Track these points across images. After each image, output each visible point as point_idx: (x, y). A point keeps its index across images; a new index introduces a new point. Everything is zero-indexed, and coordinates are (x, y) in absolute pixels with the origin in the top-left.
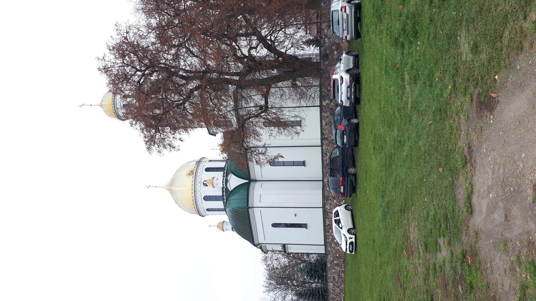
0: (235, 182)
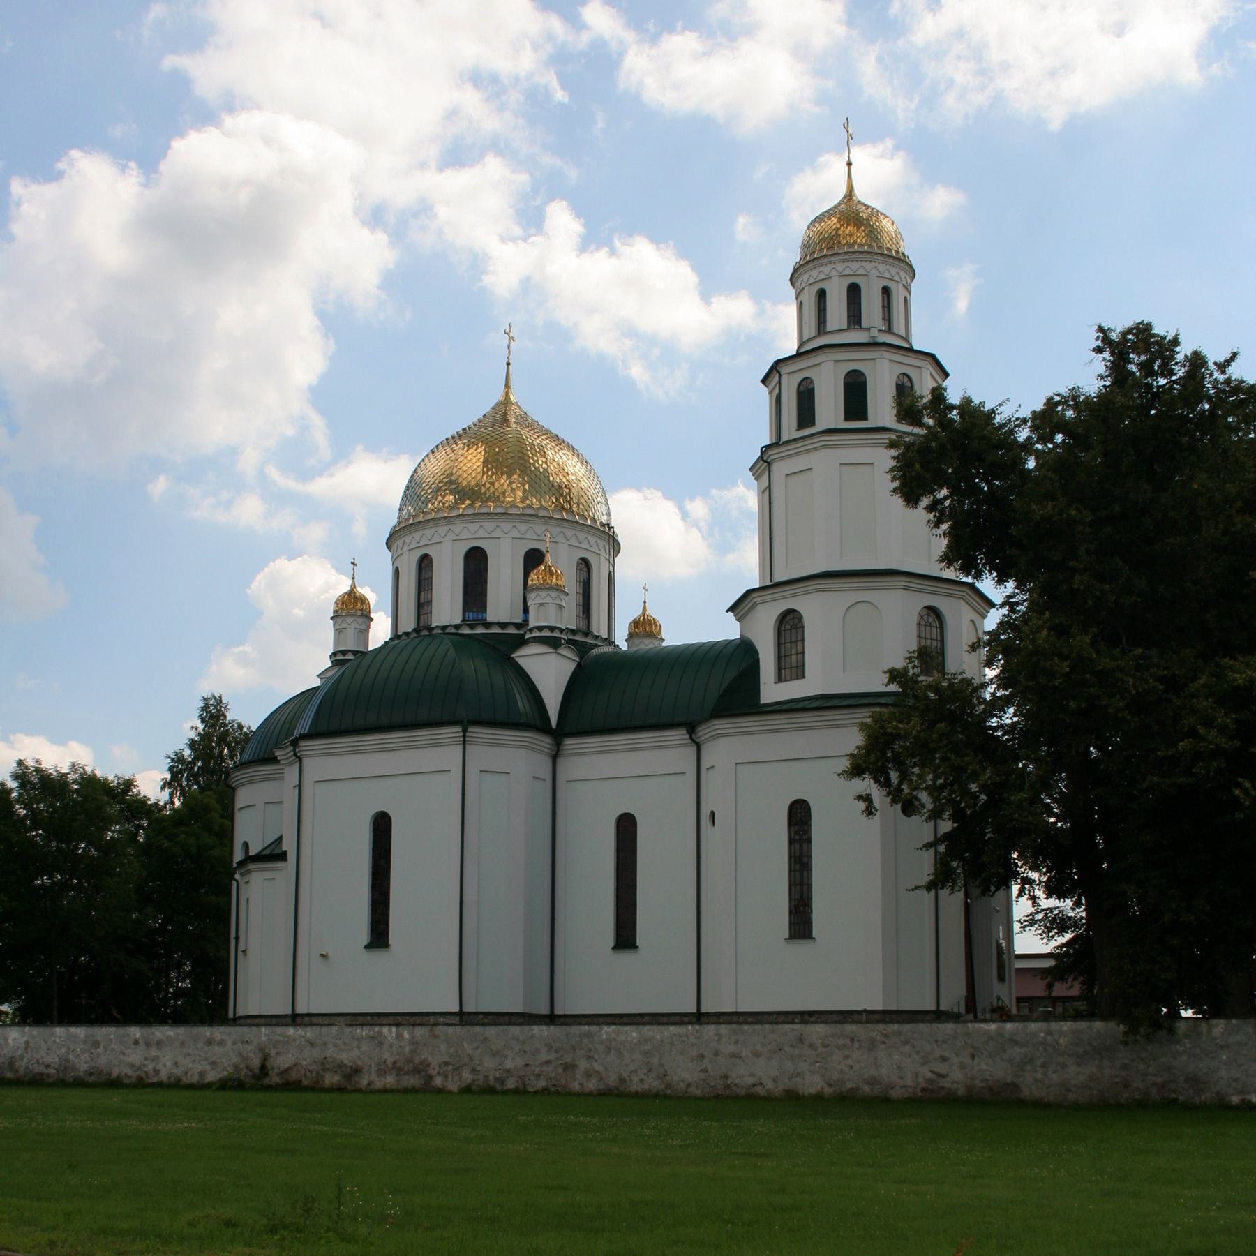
0: (550, 673)
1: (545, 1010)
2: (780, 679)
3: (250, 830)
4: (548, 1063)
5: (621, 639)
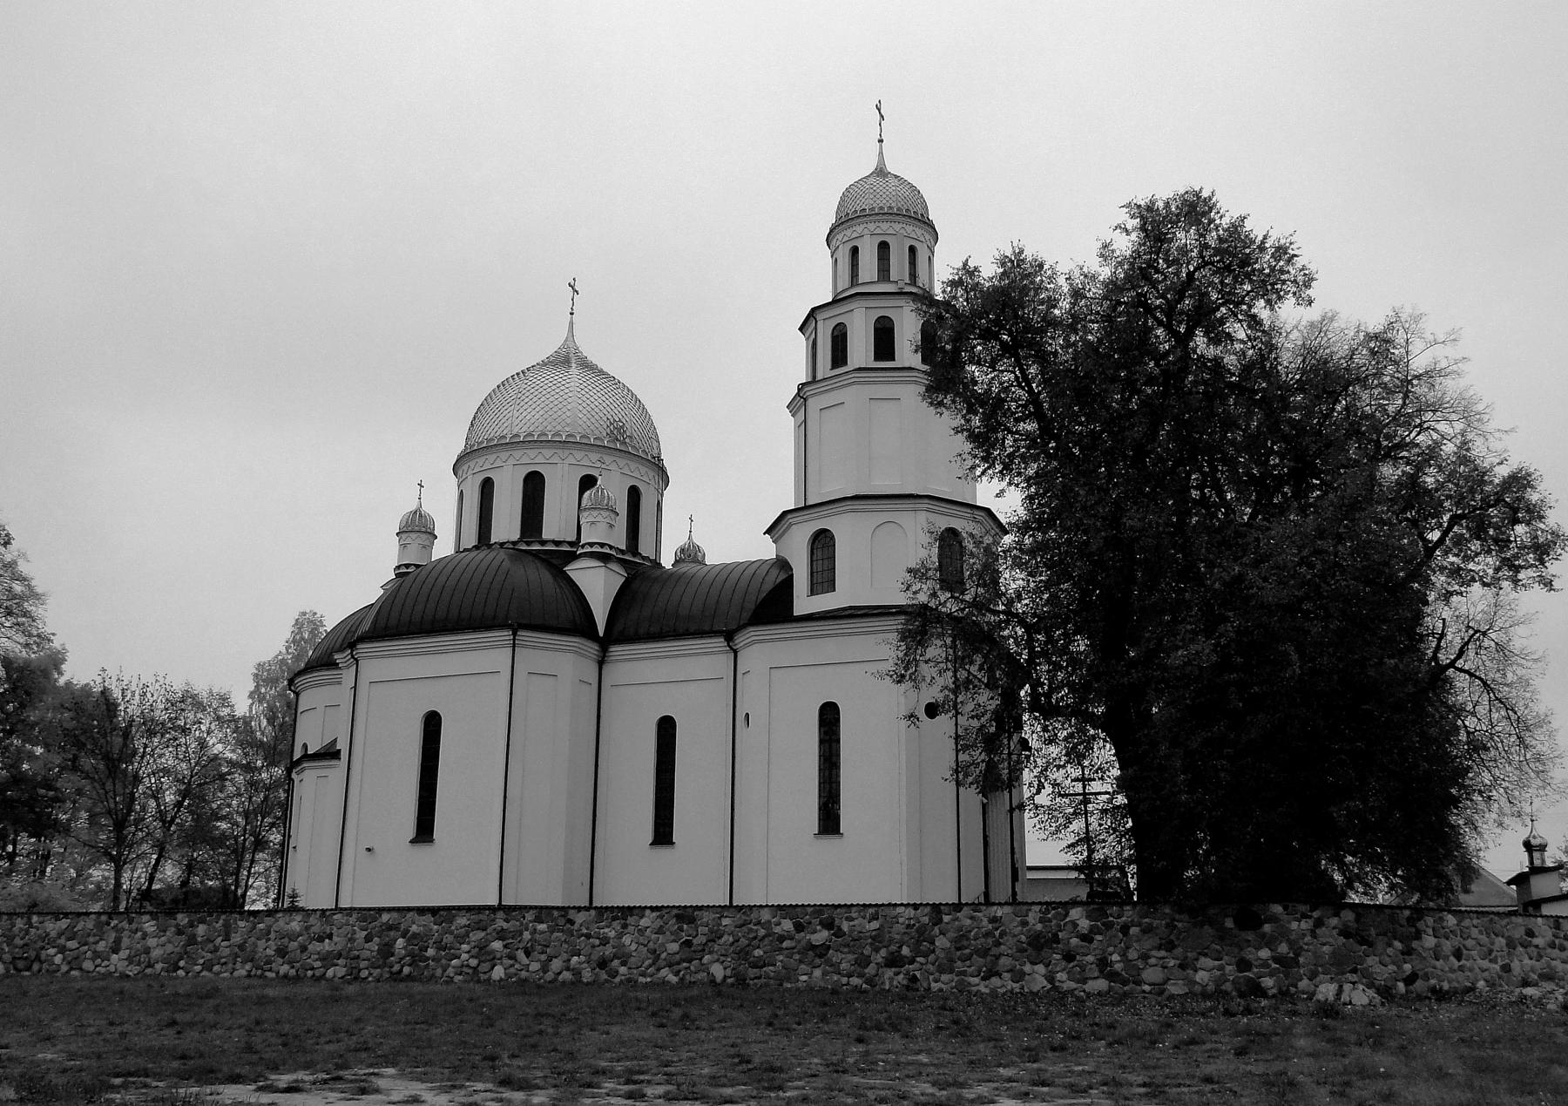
0: (598, 586)
2: (813, 592)
3: (310, 735)
5: (667, 561)
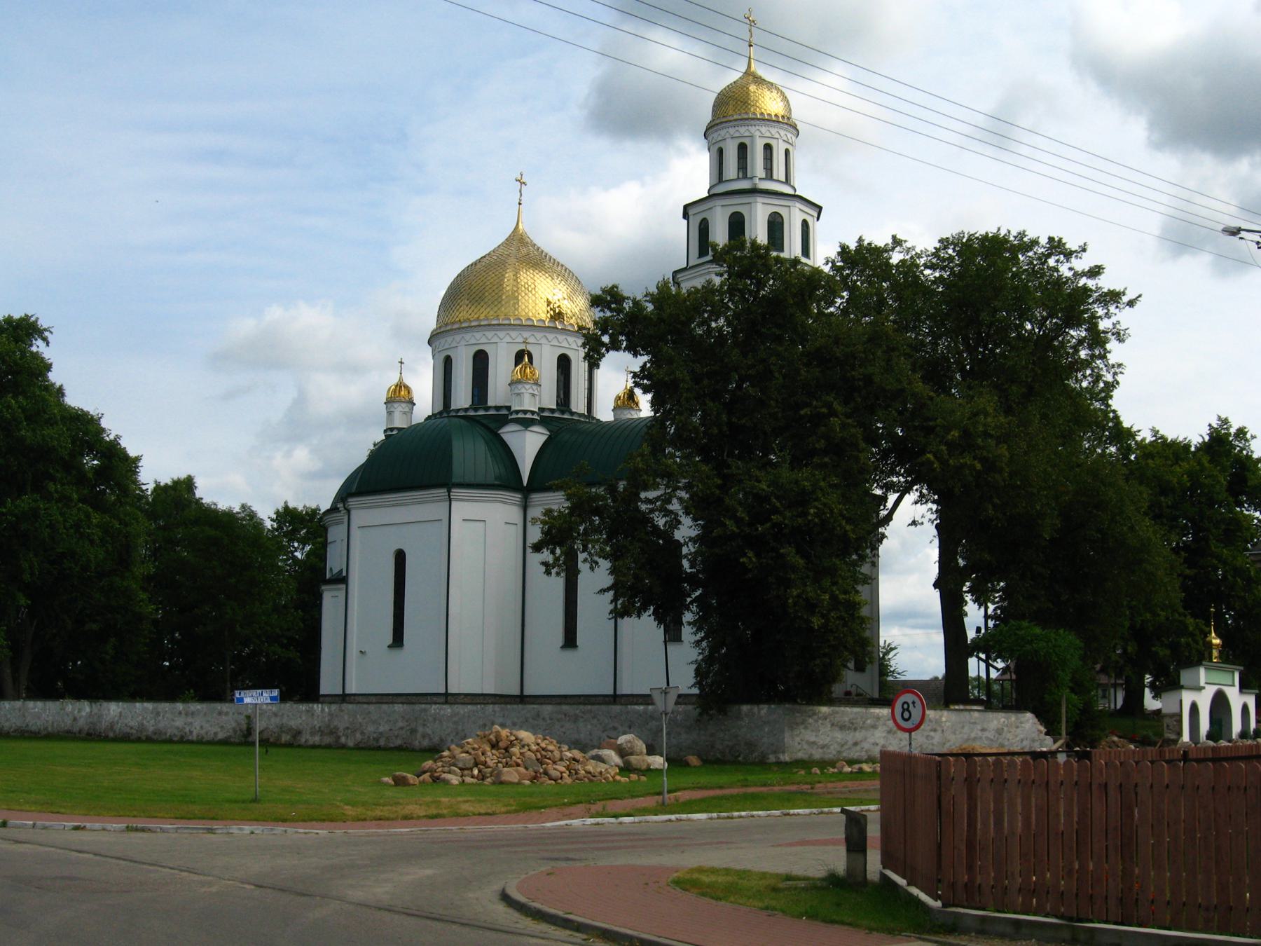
0: (527, 445)
1: (515, 691)
4: (402, 728)
